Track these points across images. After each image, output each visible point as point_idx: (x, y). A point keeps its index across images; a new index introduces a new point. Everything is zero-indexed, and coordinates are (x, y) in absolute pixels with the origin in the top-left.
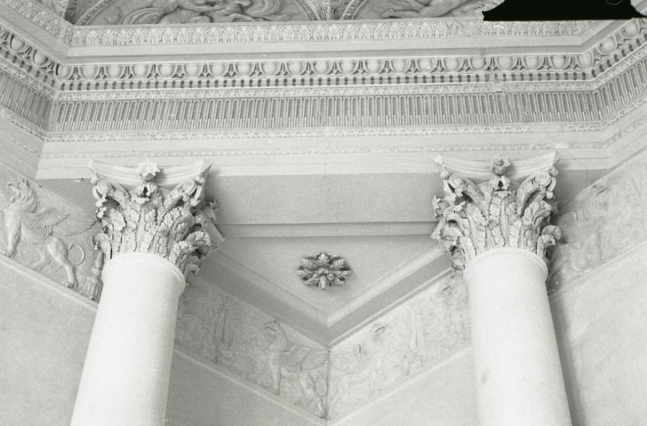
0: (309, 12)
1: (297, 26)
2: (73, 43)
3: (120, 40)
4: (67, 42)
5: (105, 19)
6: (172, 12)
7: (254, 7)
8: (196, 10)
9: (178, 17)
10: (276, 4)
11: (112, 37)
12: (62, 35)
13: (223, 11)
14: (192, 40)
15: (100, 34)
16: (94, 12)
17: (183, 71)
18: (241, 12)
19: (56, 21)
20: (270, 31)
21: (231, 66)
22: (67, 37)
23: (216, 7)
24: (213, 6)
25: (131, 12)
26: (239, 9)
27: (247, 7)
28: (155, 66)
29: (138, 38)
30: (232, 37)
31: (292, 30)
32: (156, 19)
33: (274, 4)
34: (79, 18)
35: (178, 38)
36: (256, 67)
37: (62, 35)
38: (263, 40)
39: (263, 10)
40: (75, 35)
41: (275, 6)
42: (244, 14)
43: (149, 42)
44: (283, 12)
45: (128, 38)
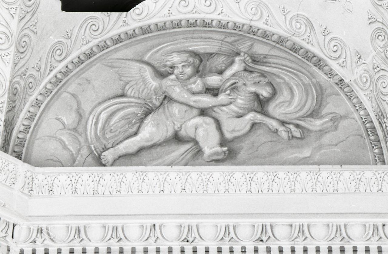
0: (362, 113)
1: (358, 172)
2: (34, 193)
3: (103, 189)
4: (26, 191)
5: (58, 119)
6: (158, 108)
7: (279, 99)
8: (192, 103)
9: (167, 119)
10: (310, 95)
11: (91, 184)
12: (19, 184)
13: (232, 107)
14: (206, 191)
15: (73, 179)
16: (38, 103)
17: (195, 234)
18: (260, 110)
19: (11, 167)
20: (320, 179)
21: (264, 227)
22: (26, 186)
23: (222, 98)
24: (216, 95)
25: (95, 107)
26: (256, 104)
27: (268, 100)
28: (154, 225)
29: (129, 187)
30: (265, 187)
31: (352, 178)
32: (135, 124)
33: (307, 95)
34: (18, 117)
35: (188, 187)
36: (301, 231)
37: (19, 184)
38: (310, 191)
39: (292, 108)
40: (36, 181)
41: (310, 98)
42: (265, 114)
43: (145, 192)
44: (323, 112)
45: (114, 187)
